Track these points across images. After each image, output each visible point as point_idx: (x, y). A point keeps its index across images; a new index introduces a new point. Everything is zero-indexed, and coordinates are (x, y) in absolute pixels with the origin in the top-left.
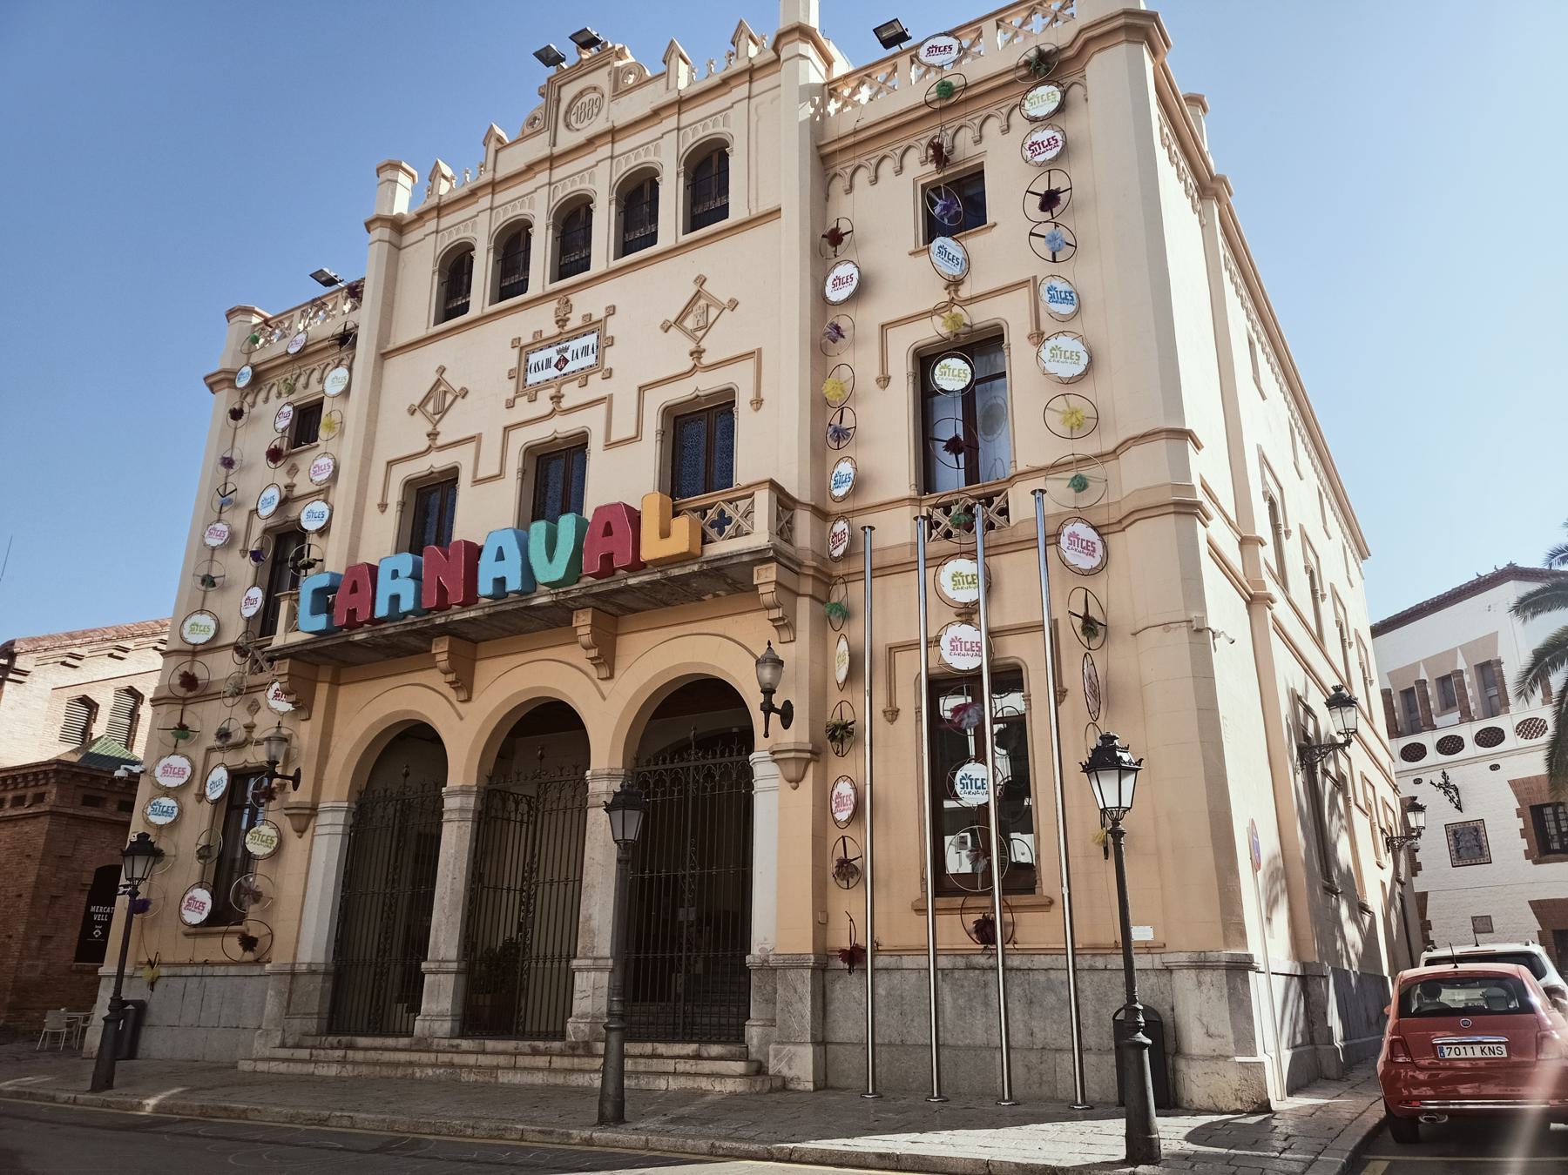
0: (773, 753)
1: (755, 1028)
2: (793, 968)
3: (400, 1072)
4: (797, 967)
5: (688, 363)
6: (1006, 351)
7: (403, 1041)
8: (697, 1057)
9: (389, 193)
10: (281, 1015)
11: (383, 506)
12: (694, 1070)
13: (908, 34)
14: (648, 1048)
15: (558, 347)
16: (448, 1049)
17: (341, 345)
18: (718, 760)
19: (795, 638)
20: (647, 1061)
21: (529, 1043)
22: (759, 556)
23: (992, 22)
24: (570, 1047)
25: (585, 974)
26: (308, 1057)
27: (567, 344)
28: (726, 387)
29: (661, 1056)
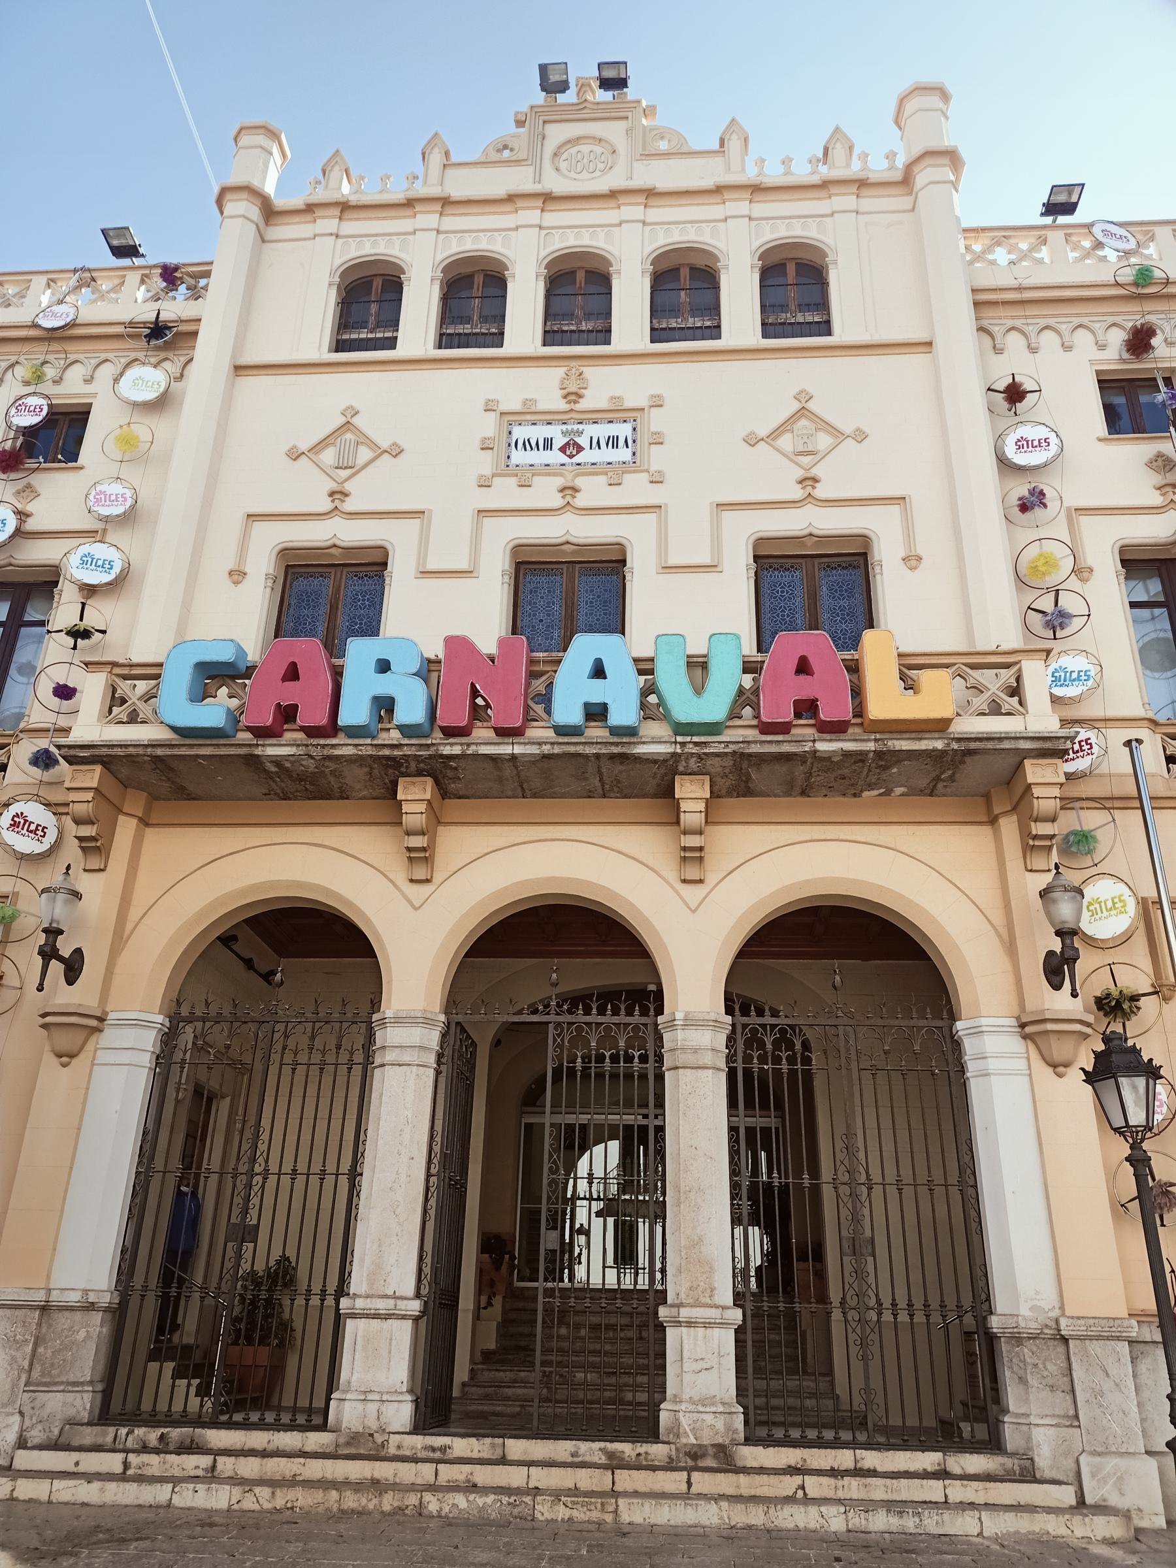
0: (44, 1016)
1: (1041, 1429)
2: (1099, 1338)
3: (388, 1502)
4: (1108, 1338)
5: (326, 505)
6: (56, 596)
7: (315, 1440)
8: (942, 1474)
9: (261, 164)
10: (14, 1385)
11: (237, 575)
12: (980, 1499)
13: (141, 250)
14: (844, 1458)
15: (564, 427)
16: (422, 1454)
17: (149, 337)
18: (622, 1018)
19: (106, 867)
20: (888, 1481)
21: (602, 1445)
22: (1048, 745)
23: (43, 279)
24: (688, 1454)
25: (701, 1331)
26: (119, 1469)
27: (581, 427)
28: (379, 543)
29: (872, 1473)
